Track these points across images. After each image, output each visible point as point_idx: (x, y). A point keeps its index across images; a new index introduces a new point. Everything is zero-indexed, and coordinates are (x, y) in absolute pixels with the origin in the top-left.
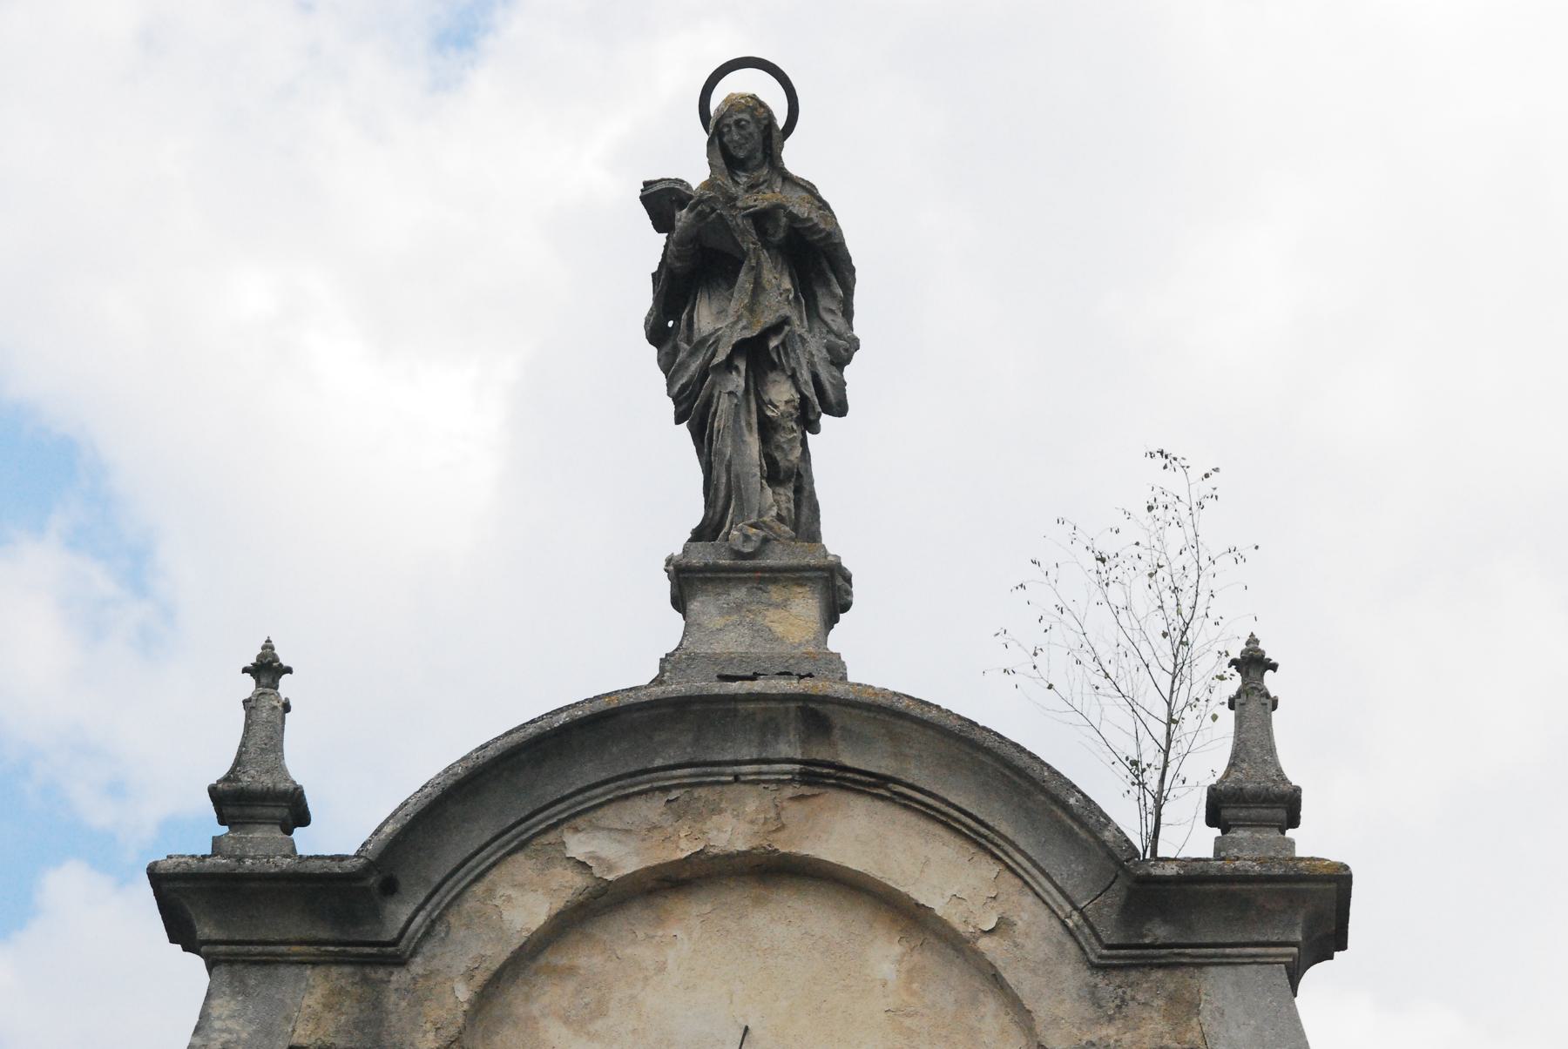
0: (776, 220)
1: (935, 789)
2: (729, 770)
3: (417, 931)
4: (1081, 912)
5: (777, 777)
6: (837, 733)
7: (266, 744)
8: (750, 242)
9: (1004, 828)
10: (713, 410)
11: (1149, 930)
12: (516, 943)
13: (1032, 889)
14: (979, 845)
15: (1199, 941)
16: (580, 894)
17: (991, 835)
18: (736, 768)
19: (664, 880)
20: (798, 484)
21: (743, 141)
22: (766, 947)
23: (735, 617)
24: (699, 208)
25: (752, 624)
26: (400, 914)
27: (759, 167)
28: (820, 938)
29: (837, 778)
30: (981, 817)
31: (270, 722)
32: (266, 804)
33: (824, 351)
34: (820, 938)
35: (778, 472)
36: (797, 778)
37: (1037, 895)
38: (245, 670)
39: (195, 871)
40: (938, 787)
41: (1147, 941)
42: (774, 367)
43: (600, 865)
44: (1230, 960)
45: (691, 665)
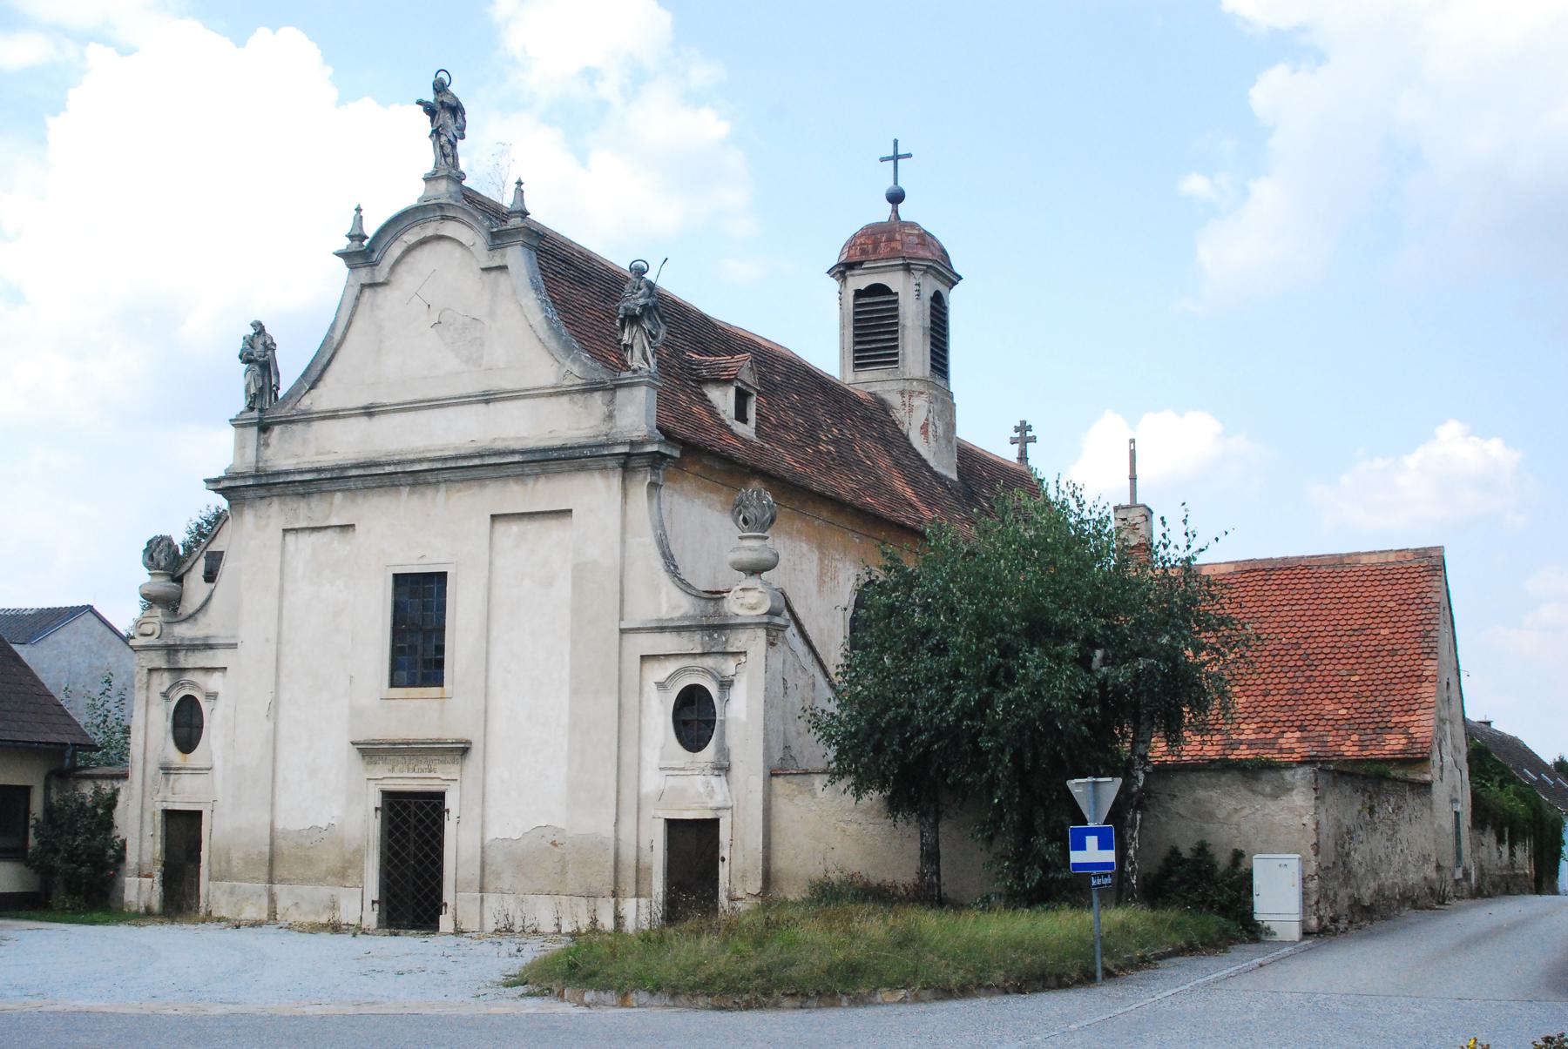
26: (375, 256)
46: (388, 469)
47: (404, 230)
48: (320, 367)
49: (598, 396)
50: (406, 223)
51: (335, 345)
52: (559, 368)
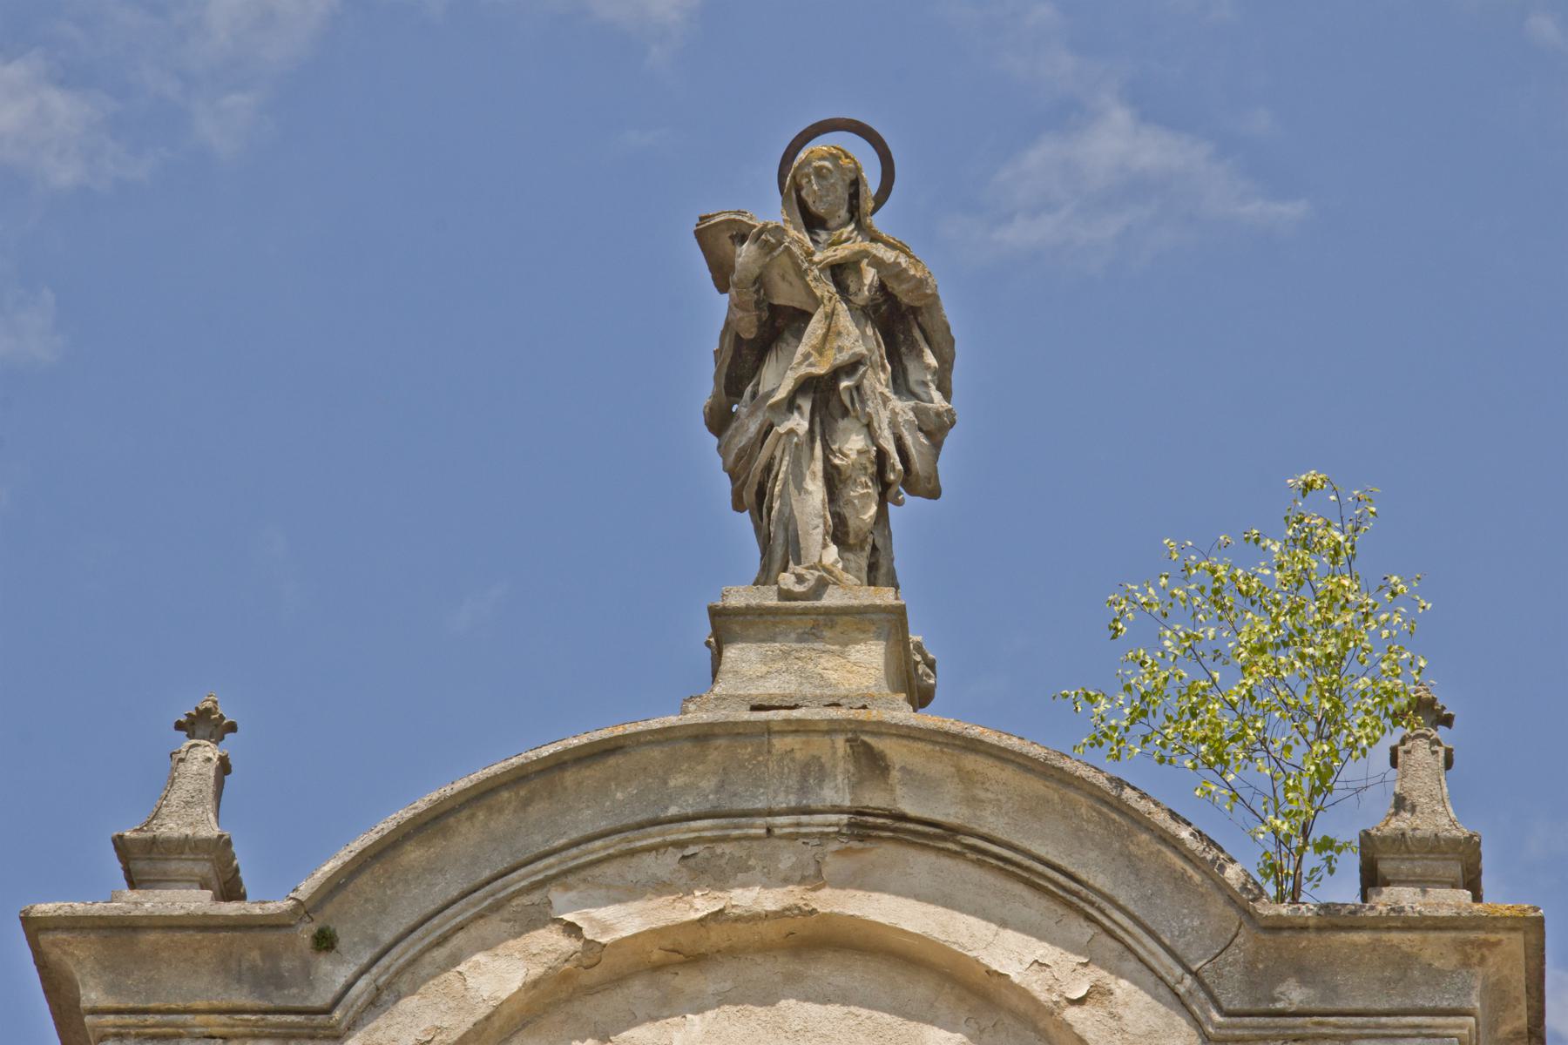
0: (859, 273)
1: (1016, 840)
2: (759, 821)
3: (358, 997)
4: (1195, 975)
5: (820, 829)
6: (895, 774)
7: (193, 797)
8: (825, 289)
9: (1100, 881)
10: (774, 473)
11: (1281, 993)
12: (482, 1012)
14: (1069, 905)
15: (1348, 1007)
16: (566, 961)
17: (1084, 892)
18: (769, 819)
19: (673, 951)
20: (873, 560)
21: (824, 193)
22: (799, 1027)
23: (780, 665)
24: (763, 237)
25: (802, 670)
27: (844, 225)
28: (867, 1018)
29: (894, 830)
30: (1071, 869)
31: (201, 775)
32: (183, 857)
33: (911, 414)
34: (867, 1018)
36: (844, 830)
37: (1141, 960)
38: (179, 726)
39: (80, 913)
40: (1020, 836)
41: (1279, 1006)
42: (845, 413)
43: (591, 926)
44: (1387, 1032)
45: (720, 705)
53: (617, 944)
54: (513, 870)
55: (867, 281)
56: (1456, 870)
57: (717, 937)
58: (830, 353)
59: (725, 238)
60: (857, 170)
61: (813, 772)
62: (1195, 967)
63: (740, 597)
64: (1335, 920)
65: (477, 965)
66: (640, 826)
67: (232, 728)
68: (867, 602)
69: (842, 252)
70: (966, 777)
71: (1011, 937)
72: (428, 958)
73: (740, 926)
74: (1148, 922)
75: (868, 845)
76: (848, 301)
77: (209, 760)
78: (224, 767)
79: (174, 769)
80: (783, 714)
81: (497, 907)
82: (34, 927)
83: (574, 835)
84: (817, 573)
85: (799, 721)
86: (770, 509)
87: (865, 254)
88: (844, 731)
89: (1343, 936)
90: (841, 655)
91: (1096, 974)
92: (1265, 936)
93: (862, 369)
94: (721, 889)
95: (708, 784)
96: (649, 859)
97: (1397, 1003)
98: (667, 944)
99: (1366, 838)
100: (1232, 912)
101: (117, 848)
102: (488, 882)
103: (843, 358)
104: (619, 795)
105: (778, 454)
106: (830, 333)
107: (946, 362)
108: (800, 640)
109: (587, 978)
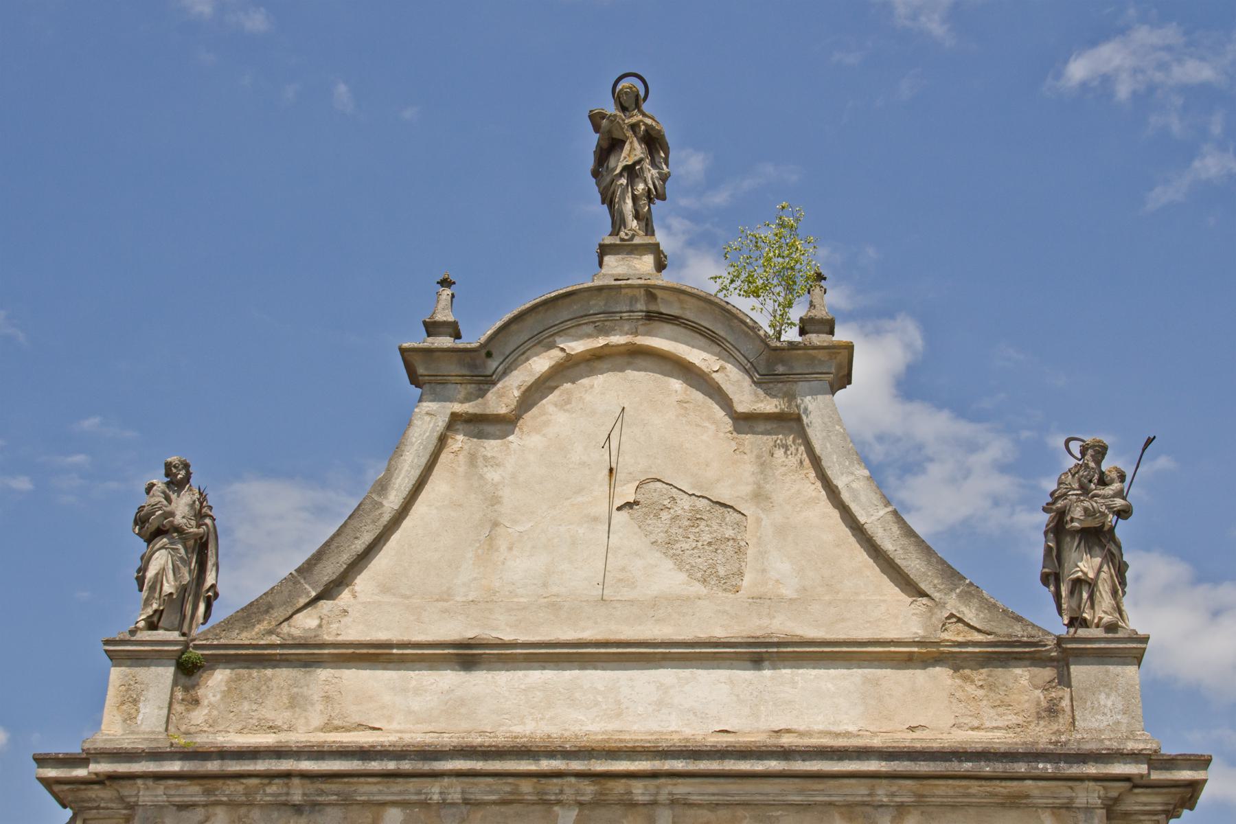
0: (640, 127)
4: (751, 363)
6: (659, 300)
8: (629, 134)
9: (722, 333)
12: (537, 376)
13: (733, 356)
14: (713, 341)
17: (717, 337)
18: (621, 315)
23: (621, 263)
26: (493, 364)
27: (634, 110)
35: (639, 216)
38: (438, 283)
41: (776, 372)
42: (638, 177)
46: (546, 765)
47: (564, 330)
48: (345, 558)
49: (1021, 676)
50: (565, 315)
51: (386, 518)
52: (930, 610)
53: (577, 354)
54: (544, 331)
55: (642, 129)
56: (827, 328)
57: (607, 351)
58: (632, 156)
59: (598, 118)
60: (638, 91)
61: (634, 299)
62: (751, 361)
63: (609, 240)
64: (793, 347)
65: (535, 361)
66: (582, 317)
67: (454, 283)
68: (647, 242)
69: (634, 120)
70: (681, 301)
71: (696, 351)
72: (519, 359)
73: (613, 348)
74: (736, 346)
75: (651, 322)
76: (636, 136)
77: (448, 295)
78: (453, 296)
79: (438, 298)
80: (624, 282)
81: (539, 342)
82: (403, 351)
83: (562, 320)
84: (632, 232)
85: (630, 284)
86: (614, 206)
87: (642, 121)
88: (644, 287)
89: (795, 352)
90: (640, 259)
91: (721, 362)
92: (773, 352)
93: (643, 162)
94: (607, 336)
95: (602, 303)
96: (584, 327)
97: (810, 371)
98: (591, 353)
99: (801, 319)
100: (762, 344)
101: (424, 324)
102: (536, 335)
103: (636, 158)
104: (575, 307)
105: (616, 189)
106: (632, 149)
107: (667, 154)
108: (627, 254)
109: (568, 364)
